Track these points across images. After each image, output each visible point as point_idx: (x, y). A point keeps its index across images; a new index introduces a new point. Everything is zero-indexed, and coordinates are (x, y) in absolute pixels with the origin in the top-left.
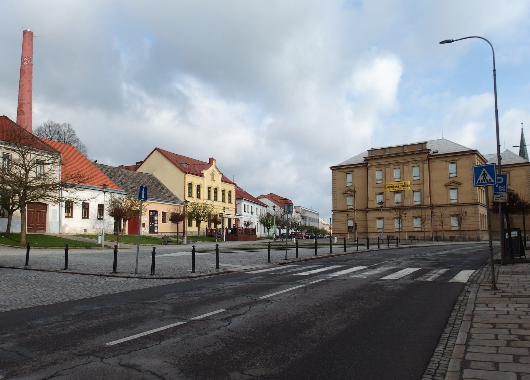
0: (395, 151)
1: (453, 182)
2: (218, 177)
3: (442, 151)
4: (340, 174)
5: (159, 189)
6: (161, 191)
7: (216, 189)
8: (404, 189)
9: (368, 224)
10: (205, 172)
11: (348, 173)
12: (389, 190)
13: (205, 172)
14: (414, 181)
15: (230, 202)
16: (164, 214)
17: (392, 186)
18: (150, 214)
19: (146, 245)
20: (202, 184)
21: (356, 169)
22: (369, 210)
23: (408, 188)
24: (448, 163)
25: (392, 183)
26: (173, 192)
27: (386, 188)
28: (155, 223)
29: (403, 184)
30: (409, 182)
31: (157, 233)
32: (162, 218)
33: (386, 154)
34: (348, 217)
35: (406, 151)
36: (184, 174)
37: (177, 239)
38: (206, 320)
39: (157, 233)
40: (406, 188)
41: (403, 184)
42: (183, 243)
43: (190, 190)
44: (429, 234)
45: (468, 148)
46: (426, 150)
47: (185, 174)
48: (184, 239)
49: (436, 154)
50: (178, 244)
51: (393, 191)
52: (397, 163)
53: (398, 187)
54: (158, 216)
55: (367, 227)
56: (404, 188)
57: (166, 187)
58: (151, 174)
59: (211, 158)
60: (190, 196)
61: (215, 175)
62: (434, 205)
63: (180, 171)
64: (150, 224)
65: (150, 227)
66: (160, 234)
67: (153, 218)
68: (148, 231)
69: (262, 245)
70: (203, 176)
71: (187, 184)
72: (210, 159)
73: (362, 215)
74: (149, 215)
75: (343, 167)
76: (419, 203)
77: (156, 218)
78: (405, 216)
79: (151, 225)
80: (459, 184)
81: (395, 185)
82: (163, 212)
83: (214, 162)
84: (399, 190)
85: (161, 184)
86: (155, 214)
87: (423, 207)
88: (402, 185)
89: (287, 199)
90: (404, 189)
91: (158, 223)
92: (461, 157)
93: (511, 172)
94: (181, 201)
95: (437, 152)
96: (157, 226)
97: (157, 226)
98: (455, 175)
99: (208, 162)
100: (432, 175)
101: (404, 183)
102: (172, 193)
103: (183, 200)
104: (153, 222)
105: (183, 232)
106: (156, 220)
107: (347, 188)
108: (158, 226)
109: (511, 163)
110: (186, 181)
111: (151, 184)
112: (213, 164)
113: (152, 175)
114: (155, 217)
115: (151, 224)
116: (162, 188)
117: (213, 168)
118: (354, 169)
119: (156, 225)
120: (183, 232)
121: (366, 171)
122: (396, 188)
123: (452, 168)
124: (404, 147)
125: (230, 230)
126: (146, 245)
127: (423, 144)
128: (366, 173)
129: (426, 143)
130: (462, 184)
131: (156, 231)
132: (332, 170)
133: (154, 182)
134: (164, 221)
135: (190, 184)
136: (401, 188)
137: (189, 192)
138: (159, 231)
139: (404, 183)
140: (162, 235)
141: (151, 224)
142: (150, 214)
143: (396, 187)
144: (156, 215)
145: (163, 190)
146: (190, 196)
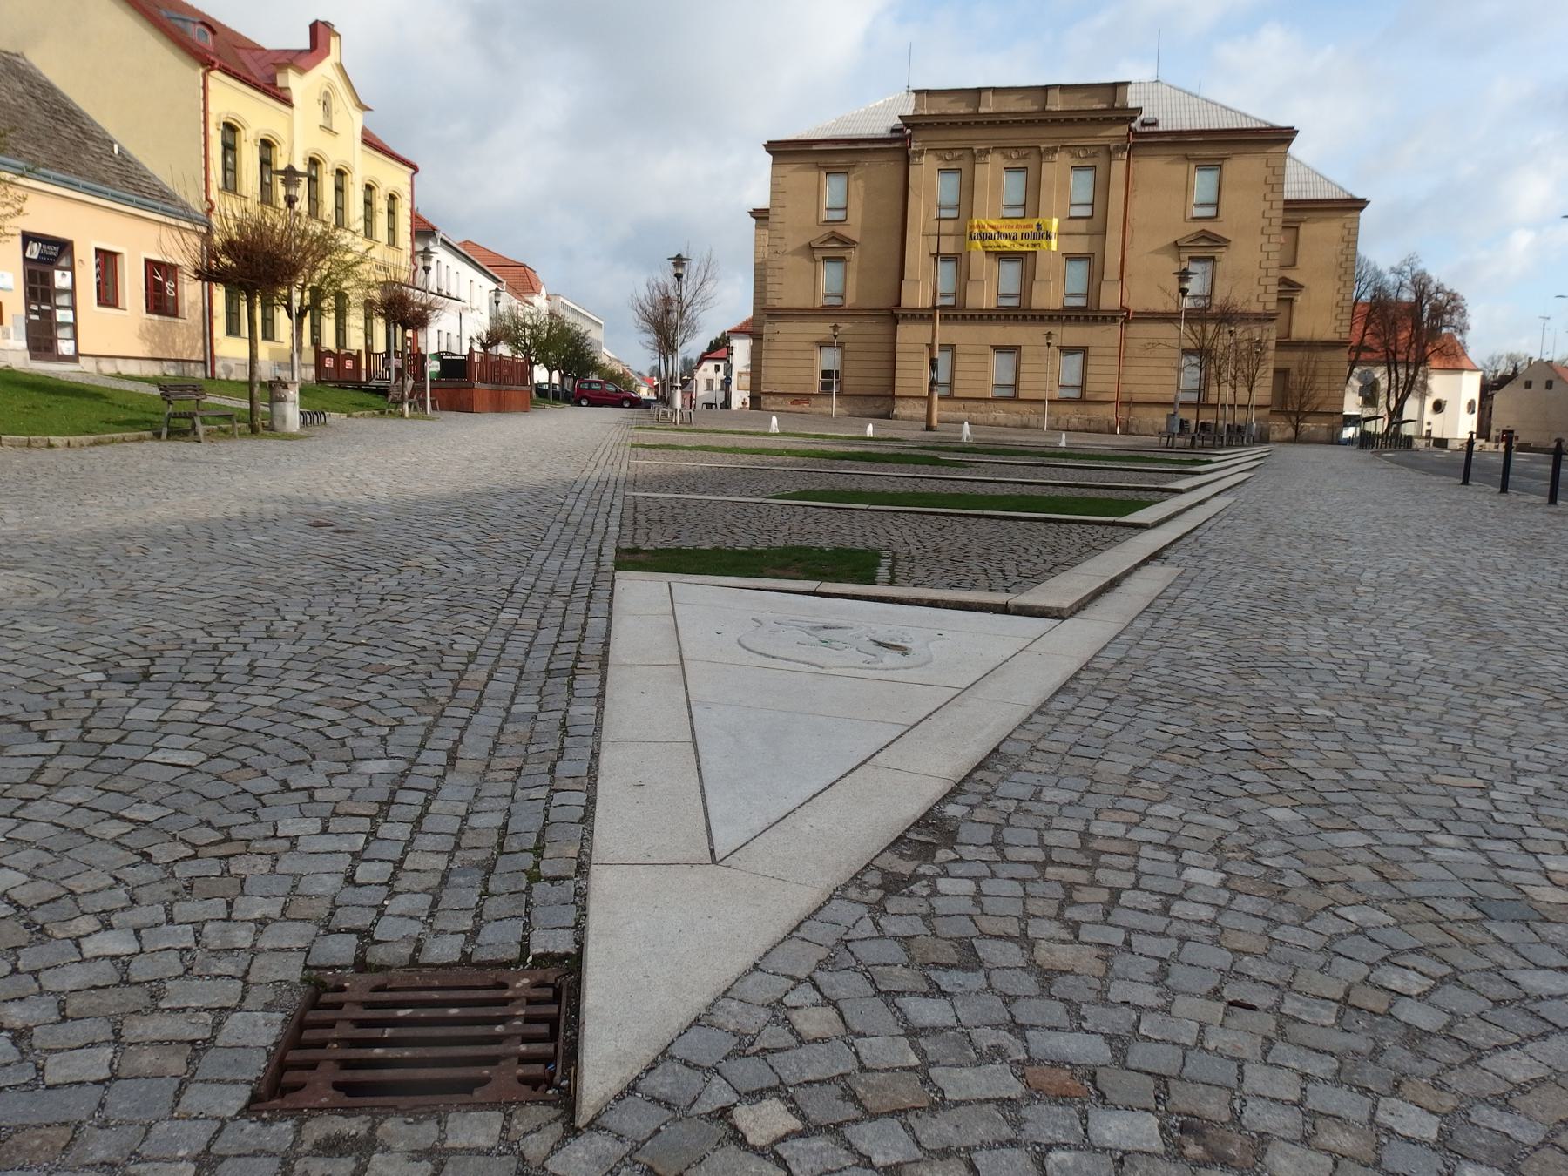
0: (1013, 105)
1: (1204, 235)
2: (351, 123)
3: (1172, 118)
4: (801, 176)
5: (68, 132)
6: (79, 145)
7: (340, 173)
8: (1034, 245)
9: (898, 365)
10: (292, 81)
11: (831, 171)
12: (980, 247)
13: (292, 81)
14: (1074, 221)
15: (392, 242)
16: (105, 260)
17: (993, 232)
18: (28, 255)
19: (55, 440)
20: (286, 139)
21: (866, 161)
22: (905, 315)
23: (1049, 245)
24: (1192, 166)
25: (993, 223)
26: (141, 159)
27: (971, 238)
28: (58, 307)
29: (1034, 229)
30: (1055, 221)
31: (75, 358)
32: (98, 283)
33: (982, 110)
34: (835, 336)
35: (1054, 108)
36: (201, 70)
37: (247, 406)
38: (451, 865)
39: (75, 358)
40: (1043, 242)
41: (1034, 229)
42: (277, 424)
43: (229, 160)
44: (1108, 413)
45: (1256, 120)
46: (1126, 109)
47: (209, 71)
48: (283, 400)
49: (1151, 129)
50: (254, 430)
51: (997, 253)
52: (1016, 148)
53: (1015, 238)
54: (72, 269)
55: (894, 377)
56: (1035, 242)
57: (106, 133)
58: (17, 55)
59: (324, 23)
60: (231, 184)
61: (336, 105)
62: (1134, 313)
63: (179, 52)
64: (29, 311)
65: (30, 325)
66: (86, 365)
67: (47, 279)
68: (24, 344)
69: (780, 453)
70: (287, 102)
71: (217, 124)
72: (314, 27)
73: (874, 331)
74: (26, 260)
75: (815, 148)
76: (1080, 302)
77: (61, 280)
78: (1049, 345)
79: (35, 313)
80: (1218, 242)
81: (1003, 231)
82: (98, 252)
83: (334, 42)
84: (1017, 248)
85: (72, 111)
86: (57, 258)
87: (1086, 318)
88: (1029, 231)
89: (523, 266)
90: (1034, 245)
91: (73, 308)
92: (1240, 149)
93: (1302, 225)
94: (186, 207)
95: (1155, 124)
96: (71, 320)
97: (71, 320)
98: (1210, 212)
99: (306, 45)
100: (1135, 204)
101: (1039, 226)
102: (138, 166)
103: (198, 207)
104: (47, 300)
105: (201, 357)
106: (63, 291)
107: (828, 229)
108: (74, 326)
109: (1304, 196)
110: (211, 108)
111: (20, 101)
112: (328, 53)
113: (22, 61)
114: (58, 274)
115: (34, 307)
116: (83, 132)
117: (325, 70)
118: (857, 157)
119: (63, 316)
120: (205, 362)
121: (901, 168)
122: (1007, 242)
123: (1203, 184)
124: (1050, 92)
125: (438, 363)
126: (50, 446)
127: (1116, 88)
128: (899, 178)
129: (1126, 84)
130: (1232, 245)
131: (66, 347)
132: (770, 158)
133: (38, 93)
134: (108, 295)
135: (230, 128)
136: (1024, 241)
137: (225, 168)
138: (81, 351)
139: (1039, 226)
140: (99, 371)
141: (34, 307)
142: (28, 255)
143: (1006, 236)
144: (64, 262)
145: (90, 143)
146: (230, 186)
